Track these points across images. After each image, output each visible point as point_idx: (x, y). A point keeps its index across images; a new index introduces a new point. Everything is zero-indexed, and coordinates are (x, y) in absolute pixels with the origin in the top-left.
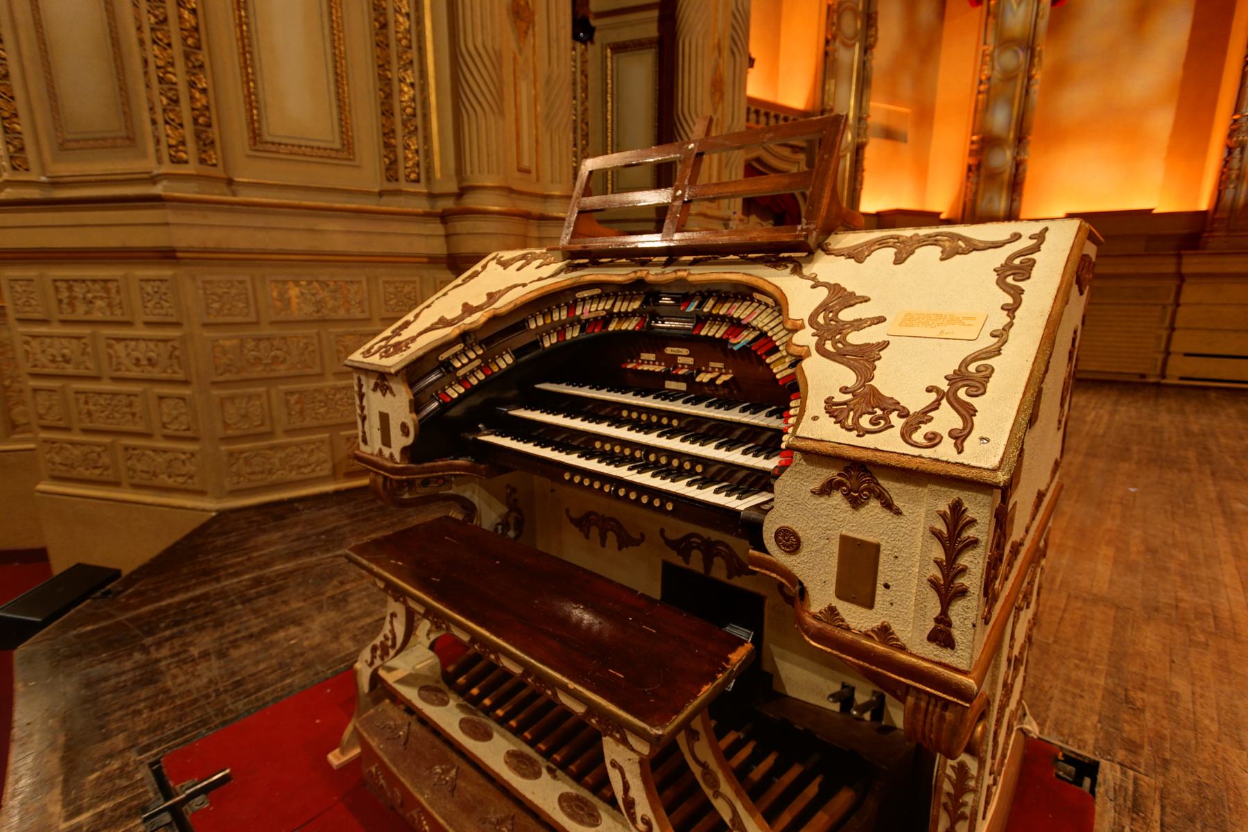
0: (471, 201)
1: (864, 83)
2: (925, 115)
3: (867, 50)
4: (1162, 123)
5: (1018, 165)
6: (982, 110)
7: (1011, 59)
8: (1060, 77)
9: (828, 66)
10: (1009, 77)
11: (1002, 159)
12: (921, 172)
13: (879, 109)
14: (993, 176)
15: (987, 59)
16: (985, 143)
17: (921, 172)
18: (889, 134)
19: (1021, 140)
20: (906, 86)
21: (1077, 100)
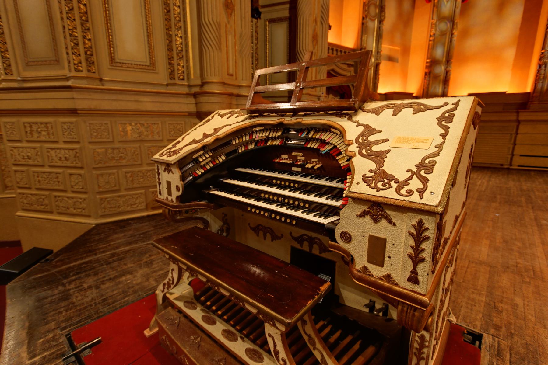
0: (207, 88)
1: (379, 37)
2: (406, 51)
3: (381, 22)
4: (510, 54)
5: (447, 72)
6: (431, 48)
7: (444, 26)
8: (465, 34)
9: (363, 29)
10: (443, 34)
11: (440, 70)
12: (405, 75)
13: (386, 48)
14: (436, 77)
15: (433, 26)
16: (433, 63)
17: (405, 75)
18: (390, 59)
19: (448, 61)
20: (398, 38)
21: (473, 44)
